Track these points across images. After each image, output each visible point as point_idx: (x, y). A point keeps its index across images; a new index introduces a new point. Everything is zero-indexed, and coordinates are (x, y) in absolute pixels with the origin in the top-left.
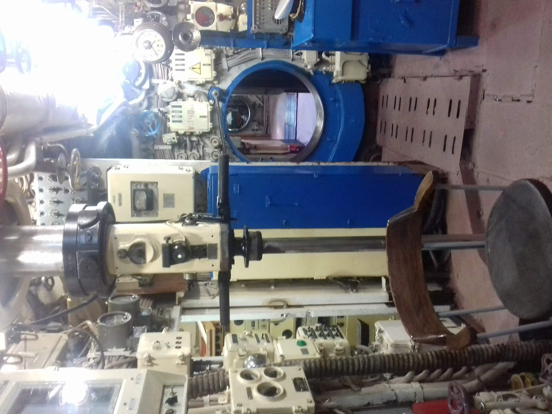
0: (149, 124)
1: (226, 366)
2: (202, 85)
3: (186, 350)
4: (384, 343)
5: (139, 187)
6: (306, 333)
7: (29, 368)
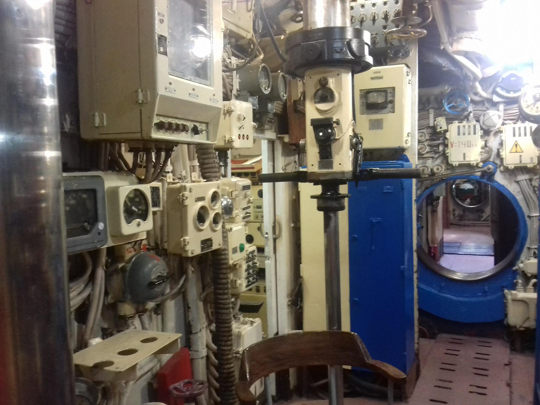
0: (456, 102)
1: (223, 180)
2: (498, 155)
3: (237, 144)
4: (242, 325)
5: (389, 95)
6: (250, 253)
7: (222, 5)
